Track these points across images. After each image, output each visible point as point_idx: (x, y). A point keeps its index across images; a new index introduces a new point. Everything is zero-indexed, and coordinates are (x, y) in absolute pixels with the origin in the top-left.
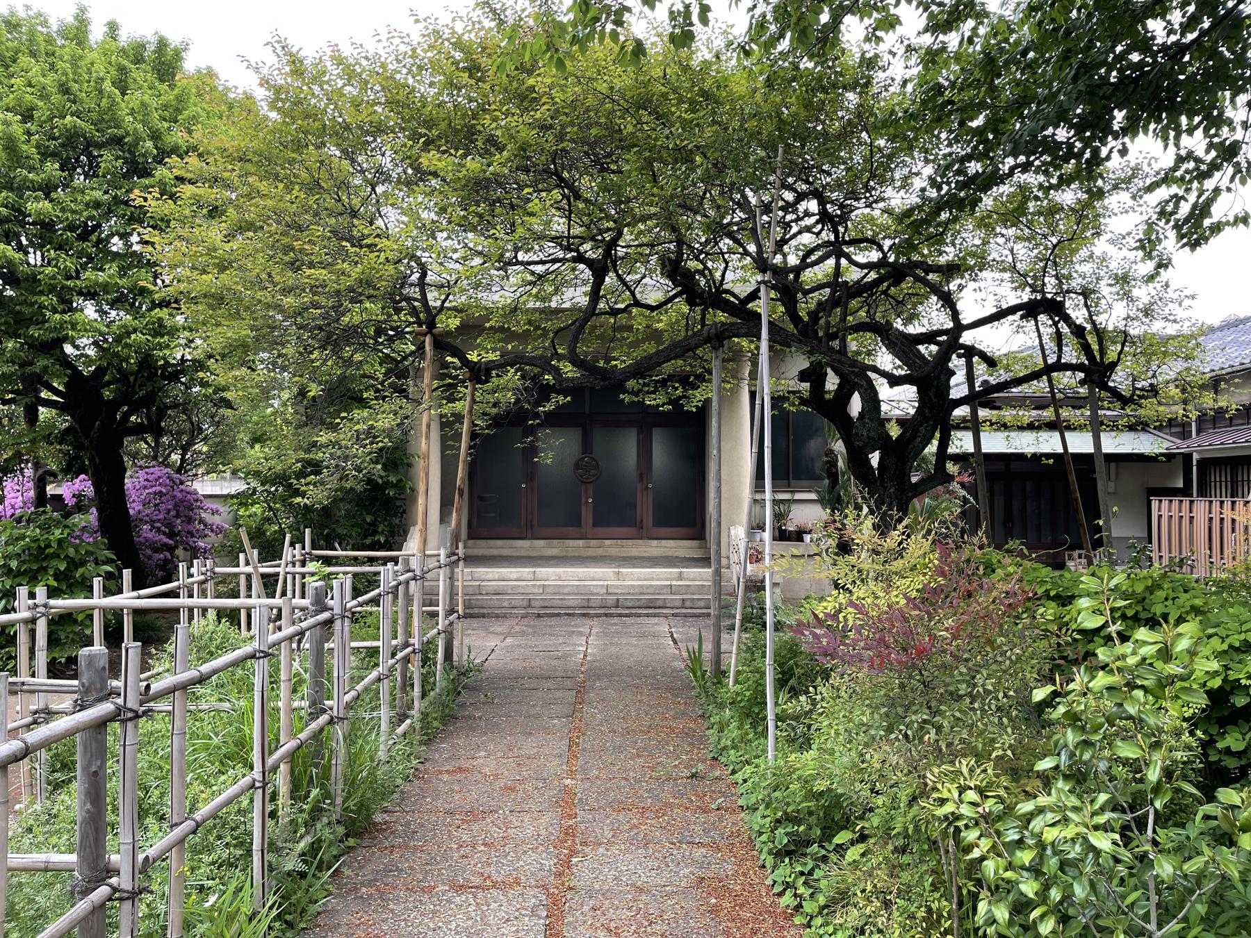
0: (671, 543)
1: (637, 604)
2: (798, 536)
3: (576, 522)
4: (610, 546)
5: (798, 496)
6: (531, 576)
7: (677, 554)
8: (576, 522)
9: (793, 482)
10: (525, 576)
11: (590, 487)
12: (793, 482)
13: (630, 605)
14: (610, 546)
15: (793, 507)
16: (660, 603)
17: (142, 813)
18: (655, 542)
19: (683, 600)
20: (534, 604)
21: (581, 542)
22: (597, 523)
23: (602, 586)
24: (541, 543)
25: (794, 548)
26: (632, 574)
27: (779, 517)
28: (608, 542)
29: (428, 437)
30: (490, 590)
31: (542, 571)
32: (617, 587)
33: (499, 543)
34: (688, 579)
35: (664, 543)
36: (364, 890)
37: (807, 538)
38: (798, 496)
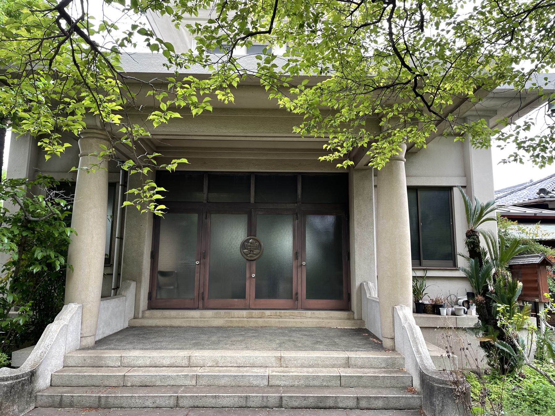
0: (323, 313)
1: (304, 403)
2: (435, 309)
3: (242, 295)
4: (270, 317)
5: (430, 274)
6: (185, 362)
7: (329, 325)
8: (242, 295)
9: (424, 262)
10: (179, 362)
11: (254, 264)
12: (424, 262)
13: (296, 404)
14: (270, 317)
15: (428, 283)
16: (331, 403)
17: (194, 299)
18: (309, 313)
19: (358, 399)
20: (182, 403)
21: (244, 313)
22: (258, 296)
23: (262, 377)
24: (209, 313)
25: (429, 319)
26: (295, 359)
27: (417, 292)
28: (268, 312)
29: (289, 372)
30: (137, 381)
31: (200, 355)
32: (279, 378)
33: (173, 313)
34: (355, 366)
35: (317, 313)
36: (357, 68)
37: (444, 311)
38: (430, 274)
